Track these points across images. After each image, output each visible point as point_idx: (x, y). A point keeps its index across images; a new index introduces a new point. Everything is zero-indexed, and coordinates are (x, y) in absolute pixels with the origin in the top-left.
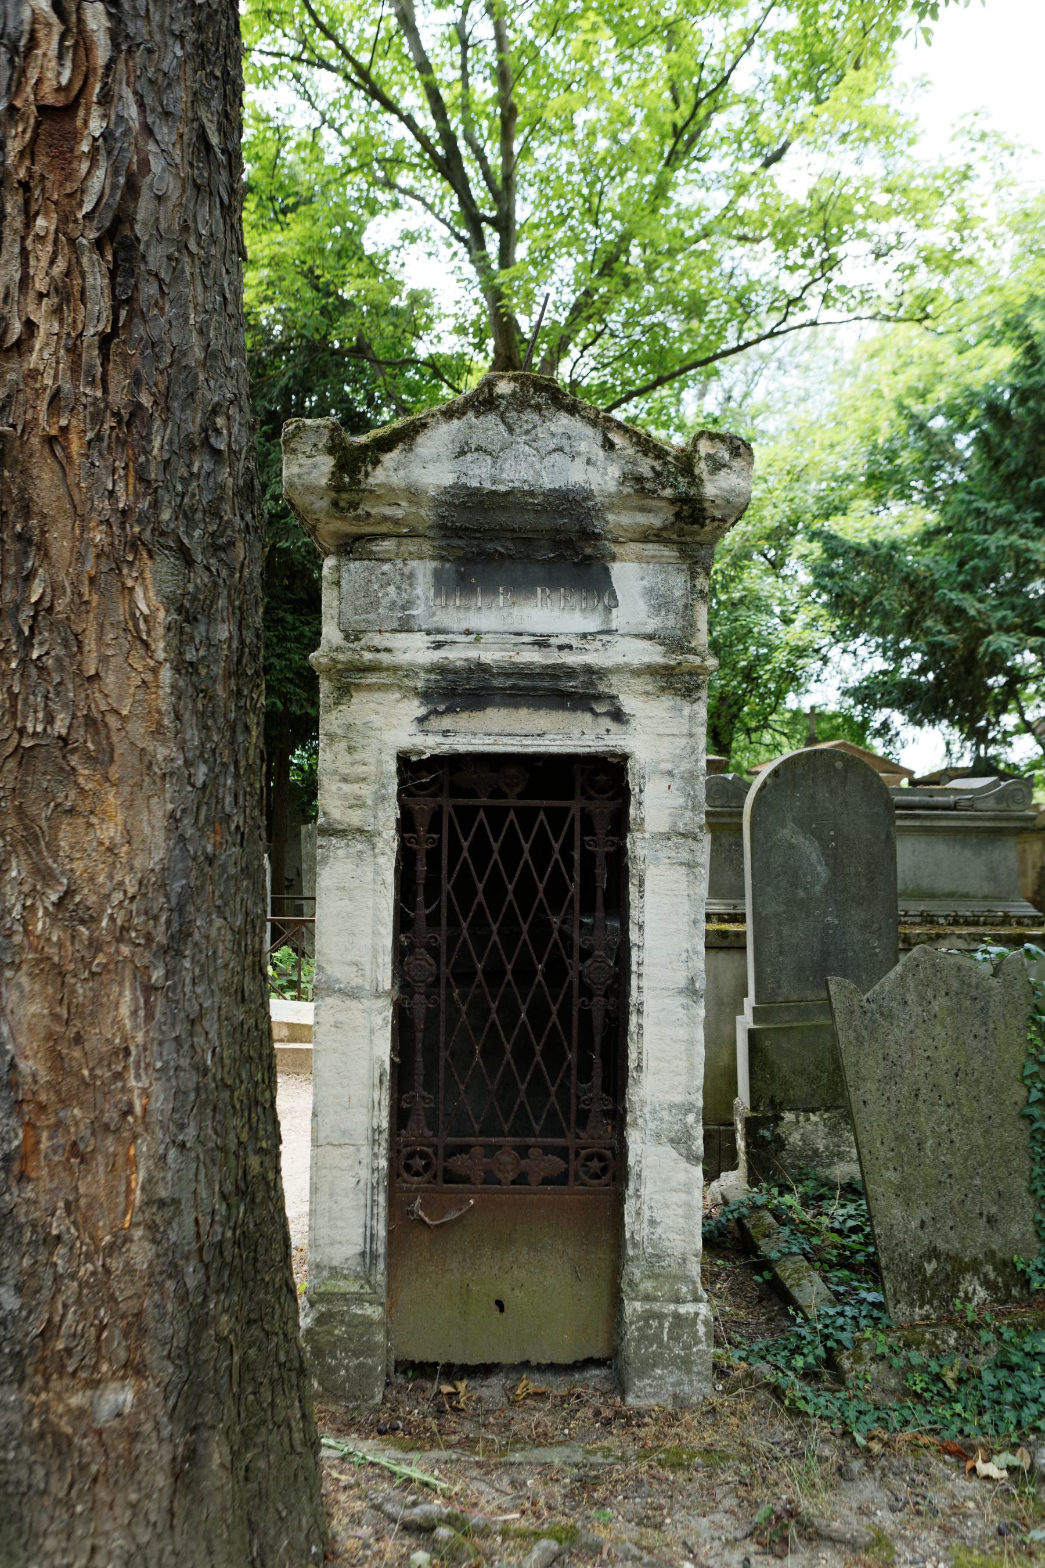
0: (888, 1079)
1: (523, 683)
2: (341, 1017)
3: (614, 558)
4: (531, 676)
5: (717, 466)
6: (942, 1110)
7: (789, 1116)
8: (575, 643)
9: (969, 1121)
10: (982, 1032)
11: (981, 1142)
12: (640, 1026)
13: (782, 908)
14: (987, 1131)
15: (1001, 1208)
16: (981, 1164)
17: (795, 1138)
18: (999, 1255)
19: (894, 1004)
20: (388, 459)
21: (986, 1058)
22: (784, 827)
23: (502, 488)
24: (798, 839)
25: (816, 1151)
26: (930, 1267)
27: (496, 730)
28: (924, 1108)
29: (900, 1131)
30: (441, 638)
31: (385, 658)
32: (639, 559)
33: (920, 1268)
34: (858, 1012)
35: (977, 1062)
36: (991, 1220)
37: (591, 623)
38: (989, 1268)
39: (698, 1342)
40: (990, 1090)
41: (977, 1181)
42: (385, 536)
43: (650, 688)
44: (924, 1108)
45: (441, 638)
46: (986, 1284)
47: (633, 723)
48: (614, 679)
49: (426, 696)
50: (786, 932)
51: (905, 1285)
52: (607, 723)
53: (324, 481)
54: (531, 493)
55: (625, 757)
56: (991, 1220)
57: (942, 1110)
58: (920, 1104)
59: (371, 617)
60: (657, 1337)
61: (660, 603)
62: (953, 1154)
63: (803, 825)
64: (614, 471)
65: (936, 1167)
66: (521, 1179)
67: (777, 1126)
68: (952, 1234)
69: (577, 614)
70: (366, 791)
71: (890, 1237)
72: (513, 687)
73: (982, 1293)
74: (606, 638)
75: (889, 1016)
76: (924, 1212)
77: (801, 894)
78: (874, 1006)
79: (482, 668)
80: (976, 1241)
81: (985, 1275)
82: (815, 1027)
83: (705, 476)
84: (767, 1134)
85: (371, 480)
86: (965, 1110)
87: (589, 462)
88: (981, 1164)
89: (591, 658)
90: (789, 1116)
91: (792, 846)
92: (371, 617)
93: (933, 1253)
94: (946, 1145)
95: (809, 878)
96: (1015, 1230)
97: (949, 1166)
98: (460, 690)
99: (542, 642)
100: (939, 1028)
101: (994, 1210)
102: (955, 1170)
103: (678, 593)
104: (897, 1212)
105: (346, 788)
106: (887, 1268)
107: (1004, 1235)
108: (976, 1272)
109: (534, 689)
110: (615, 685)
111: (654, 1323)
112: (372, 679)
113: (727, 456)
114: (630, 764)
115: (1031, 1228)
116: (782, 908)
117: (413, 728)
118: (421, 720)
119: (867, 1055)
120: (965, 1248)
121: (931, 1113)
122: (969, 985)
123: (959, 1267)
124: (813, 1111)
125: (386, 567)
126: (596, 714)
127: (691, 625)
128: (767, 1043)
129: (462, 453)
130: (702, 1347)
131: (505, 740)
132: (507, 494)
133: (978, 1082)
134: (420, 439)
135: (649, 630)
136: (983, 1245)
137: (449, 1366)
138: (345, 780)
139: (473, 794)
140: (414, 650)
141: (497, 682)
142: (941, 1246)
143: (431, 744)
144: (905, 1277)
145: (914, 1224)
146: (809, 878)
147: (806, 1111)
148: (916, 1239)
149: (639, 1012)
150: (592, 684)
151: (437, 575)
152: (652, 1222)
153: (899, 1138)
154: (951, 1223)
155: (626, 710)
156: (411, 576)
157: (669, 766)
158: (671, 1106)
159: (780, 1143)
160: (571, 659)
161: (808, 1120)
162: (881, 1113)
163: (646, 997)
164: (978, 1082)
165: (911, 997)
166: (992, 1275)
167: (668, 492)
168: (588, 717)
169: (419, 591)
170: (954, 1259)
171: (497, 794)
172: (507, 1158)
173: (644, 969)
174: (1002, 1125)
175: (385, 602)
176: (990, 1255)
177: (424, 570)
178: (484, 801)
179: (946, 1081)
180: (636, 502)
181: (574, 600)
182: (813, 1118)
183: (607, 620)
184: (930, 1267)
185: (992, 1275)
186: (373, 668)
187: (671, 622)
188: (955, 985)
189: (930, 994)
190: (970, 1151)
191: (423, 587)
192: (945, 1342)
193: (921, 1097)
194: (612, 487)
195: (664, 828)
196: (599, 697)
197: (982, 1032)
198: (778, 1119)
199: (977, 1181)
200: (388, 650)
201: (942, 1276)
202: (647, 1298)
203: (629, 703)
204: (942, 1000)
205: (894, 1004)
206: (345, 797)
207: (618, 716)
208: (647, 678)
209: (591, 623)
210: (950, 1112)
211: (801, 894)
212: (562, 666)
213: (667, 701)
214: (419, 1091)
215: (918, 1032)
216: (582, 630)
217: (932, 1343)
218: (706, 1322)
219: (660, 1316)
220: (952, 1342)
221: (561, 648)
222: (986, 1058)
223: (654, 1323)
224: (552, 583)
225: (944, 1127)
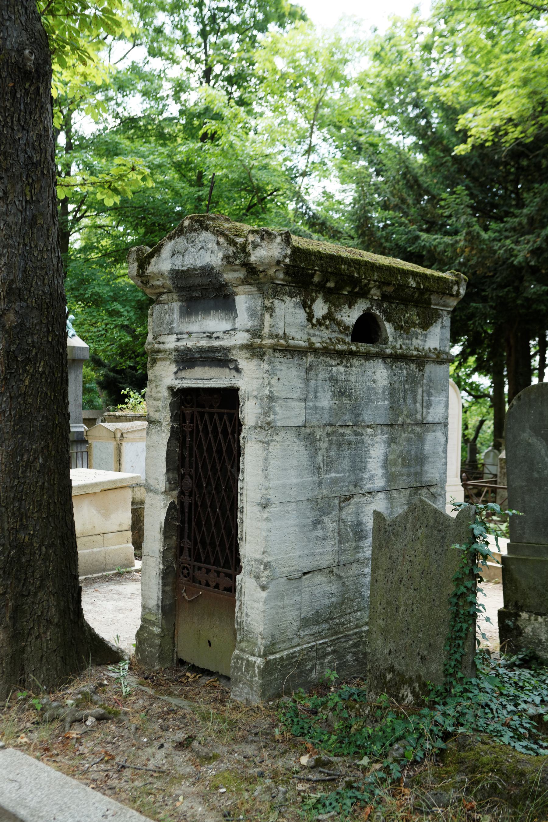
0: (390, 570)
1: (203, 355)
2: (153, 502)
3: (236, 294)
4: (205, 352)
5: (256, 246)
6: (411, 591)
7: (524, 615)
8: (221, 335)
9: (423, 600)
10: (440, 551)
11: (427, 613)
12: (242, 519)
13: (524, 484)
14: (431, 608)
15: (429, 653)
16: (425, 626)
17: (528, 630)
18: (423, 679)
19: (400, 529)
20: (153, 261)
21: (439, 566)
22: (524, 432)
23: (185, 268)
24: (533, 440)
25: (540, 640)
26: (389, 676)
27: (198, 377)
28: (403, 589)
29: (390, 599)
30: (180, 336)
31: (162, 347)
32: (245, 293)
33: (384, 675)
34: (383, 530)
35: (433, 568)
36: (423, 658)
37: (226, 325)
38: (416, 685)
39: (255, 676)
40: (437, 585)
41: (421, 635)
42: (163, 293)
43: (247, 355)
44: (403, 589)
45: (180, 336)
46: (413, 692)
47: (243, 372)
48: (234, 352)
49: (177, 361)
50: (527, 498)
51: (375, 682)
52: (234, 373)
53: (136, 273)
54: (194, 269)
55: (238, 389)
56: (423, 658)
57: (411, 591)
58: (401, 586)
59: (161, 329)
60: (241, 668)
61: (252, 314)
62: (412, 617)
63: (536, 431)
64: (220, 255)
65: (402, 622)
66: (217, 586)
67: (516, 620)
68: (402, 661)
69: (224, 322)
70: (160, 404)
71: (374, 655)
72: (201, 357)
73: (410, 698)
74: (232, 332)
75: (396, 535)
76: (392, 646)
77: (536, 475)
78: (391, 528)
79: (189, 350)
80: (413, 669)
81: (414, 688)
82: (542, 561)
83: (251, 252)
84: (510, 623)
85: (148, 271)
86: (422, 594)
87: (212, 252)
88: (425, 626)
89: (225, 343)
90: (524, 615)
91: (529, 444)
92: (161, 329)
93: (391, 669)
94: (409, 611)
95: (540, 465)
96: (434, 667)
97: (409, 624)
98: (187, 359)
99: (210, 336)
100: (419, 545)
101: (426, 653)
102: (411, 627)
103: (259, 308)
104: (380, 643)
105: (155, 403)
106: (369, 671)
107: (428, 668)
108: (410, 685)
109: (209, 358)
110: (234, 354)
111: (240, 662)
112: (160, 356)
113: (259, 240)
114: (240, 393)
115: (442, 668)
116: (524, 484)
117: (173, 377)
118: (176, 373)
119: (382, 555)
120: (407, 670)
121: (406, 592)
122: (439, 523)
123: (402, 680)
124: (541, 615)
125: (166, 306)
126: (230, 369)
127: (262, 325)
128: (513, 567)
129: (174, 255)
130: (257, 678)
131: (199, 382)
132: (188, 270)
133: (432, 579)
134: (162, 251)
135: (248, 327)
136: (417, 671)
137: (193, 666)
138: (154, 400)
139: (203, 407)
140: (170, 343)
141: (197, 355)
142: (397, 666)
143: (178, 384)
144: (376, 679)
145: (386, 651)
146: (540, 465)
147: (537, 614)
148: (385, 660)
149: (242, 512)
150: (226, 355)
151: (181, 308)
152: (247, 615)
153: (389, 603)
154: (403, 655)
155: (240, 367)
156: (173, 310)
157: (255, 393)
158: (255, 560)
159: (519, 631)
160: (217, 343)
161: (536, 620)
162: (383, 588)
163: (244, 505)
164: (432, 579)
165: (409, 526)
166: (417, 689)
167: (238, 262)
168: (227, 370)
169: (175, 316)
170: (401, 675)
171: (211, 407)
172: (212, 575)
173: (245, 492)
174: (439, 606)
175: (165, 322)
176: (419, 677)
177: (176, 306)
178: (207, 409)
179: (416, 575)
180: (229, 267)
181: (223, 315)
182: (540, 619)
183: (234, 324)
184: (389, 676)
185: (417, 689)
186: (159, 351)
187: (256, 323)
188: (432, 521)
189: (418, 525)
190: (420, 617)
191: (176, 315)
192: (364, 711)
193: (403, 582)
194: (219, 262)
195: (253, 424)
196: (231, 361)
197: (440, 551)
198: (517, 615)
199: (421, 635)
200: (163, 343)
201: (393, 683)
202: (242, 650)
203: (243, 363)
204: (423, 529)
205: (400, 529)
206: (154, 407)
207: (238, 370)
208: (245, 351)
209: (227, 326)
210: (415, 593)
211: (536, 475)
212: (212, 347)
213: (255, 362)
214: (186, 540)
215: (409, 546)
216: (224, 329)
217: (358, 710)
218: (259, 667)
219: (242, 659)
220: (367, 712)
221: (216, 338)
222: (439, 566)
223: (240, 662)
224: (216, 308)
225: (411, 601)
